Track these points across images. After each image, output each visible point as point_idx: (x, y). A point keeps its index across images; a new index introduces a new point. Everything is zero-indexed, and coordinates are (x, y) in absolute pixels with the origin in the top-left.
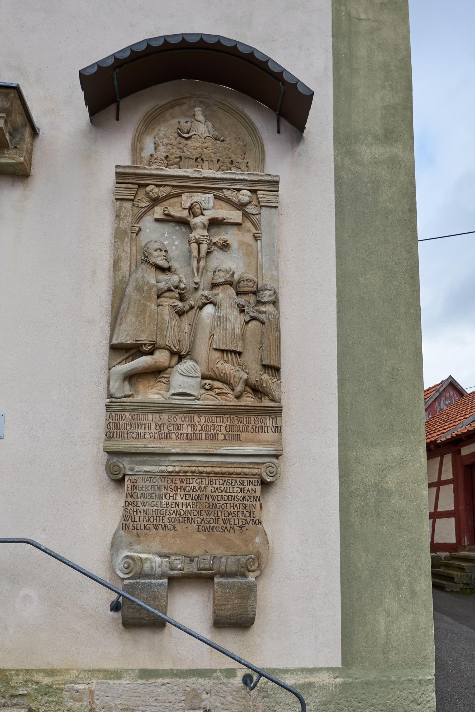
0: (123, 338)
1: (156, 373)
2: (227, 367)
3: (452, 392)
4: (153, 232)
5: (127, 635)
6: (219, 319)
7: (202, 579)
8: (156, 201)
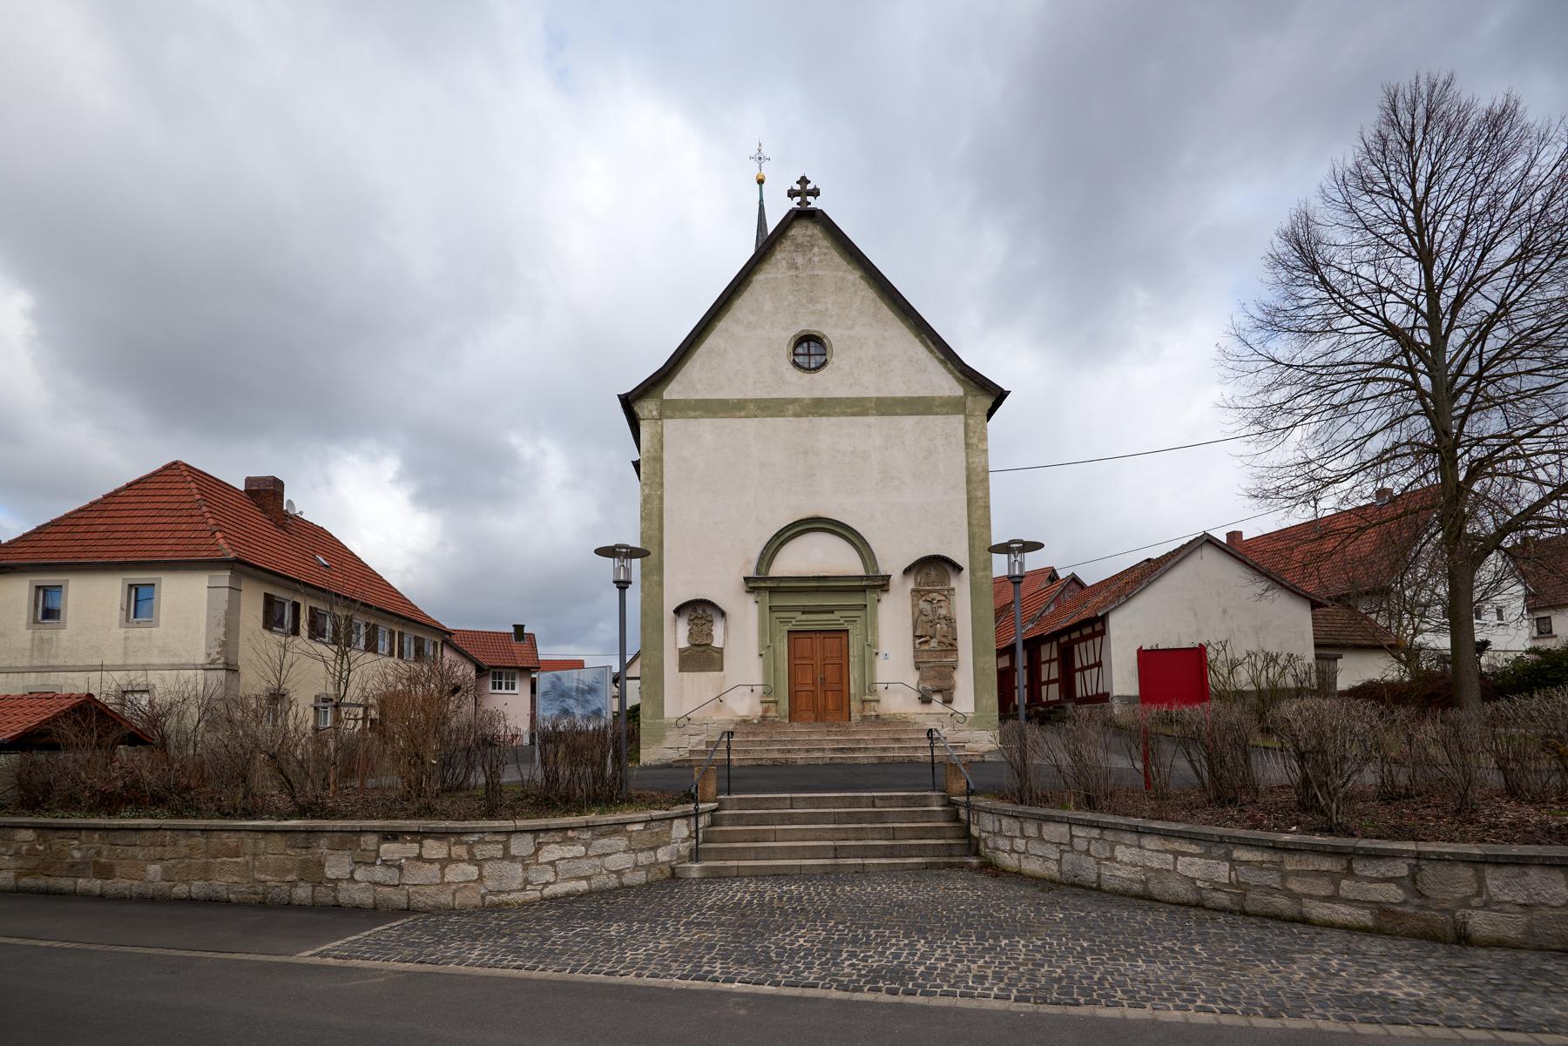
4: (922, 605)
6: (941, 627)
7: (939, 691)
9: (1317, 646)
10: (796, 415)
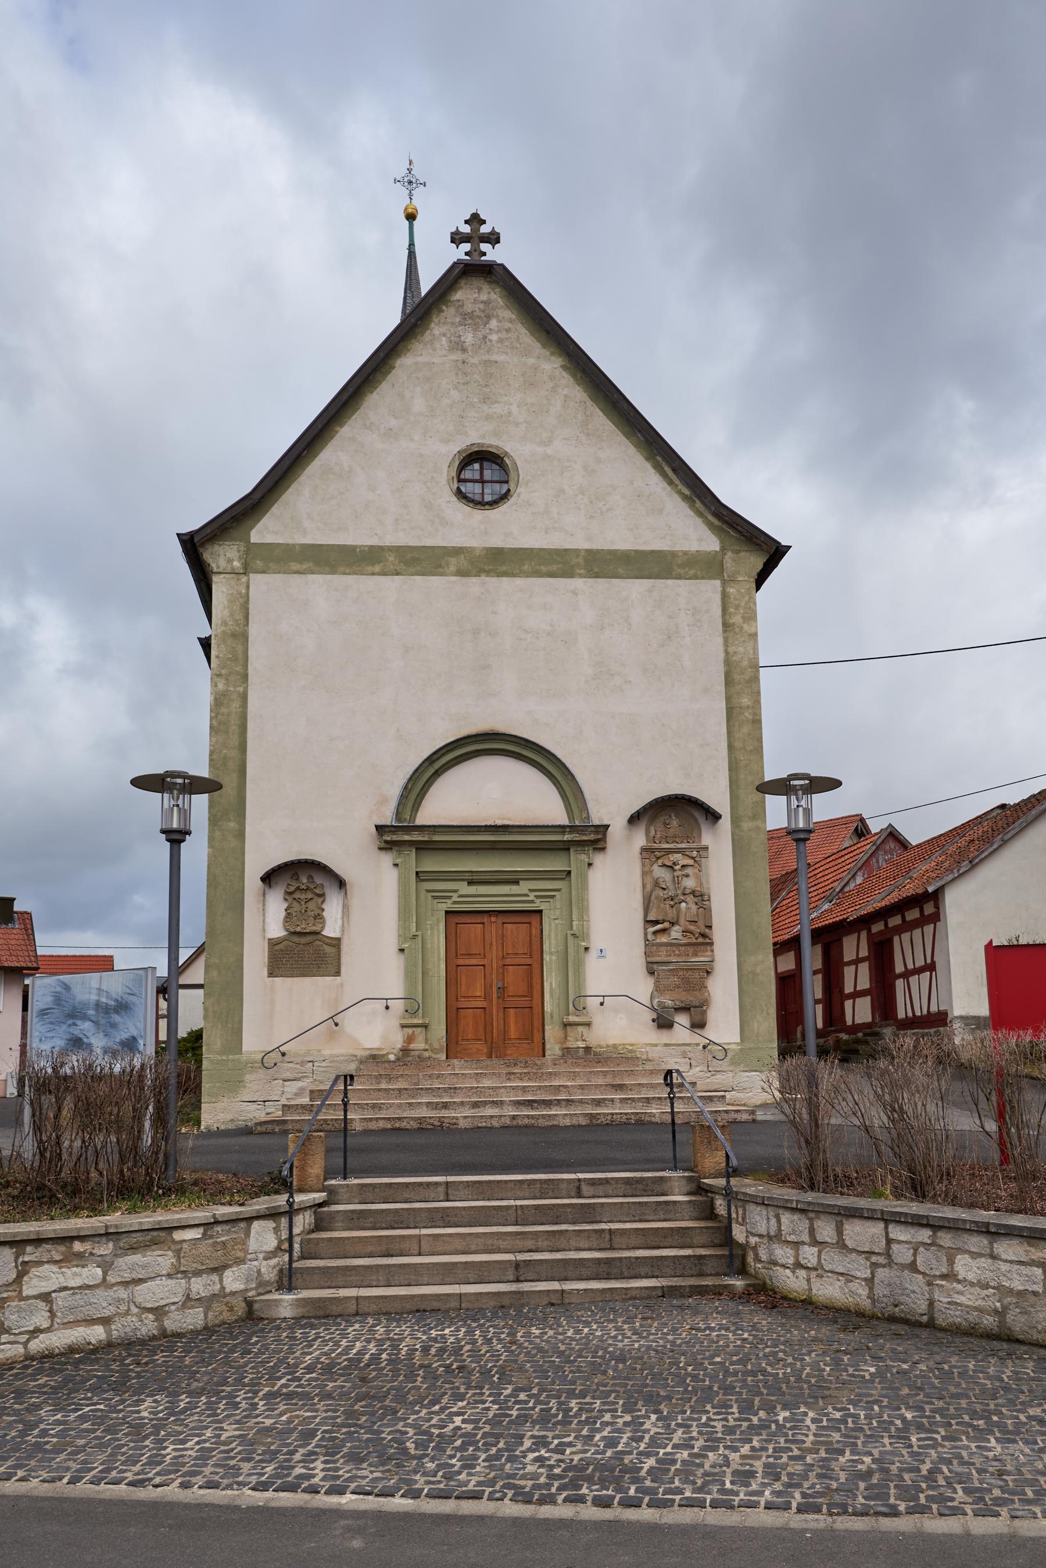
0: (651, 918)
1: (664, 931)
2: (692, 928)
3: (892, 844)
4: (659, 872)
5: (659, 1031)
8: (658, 858)
10: (462, 573)
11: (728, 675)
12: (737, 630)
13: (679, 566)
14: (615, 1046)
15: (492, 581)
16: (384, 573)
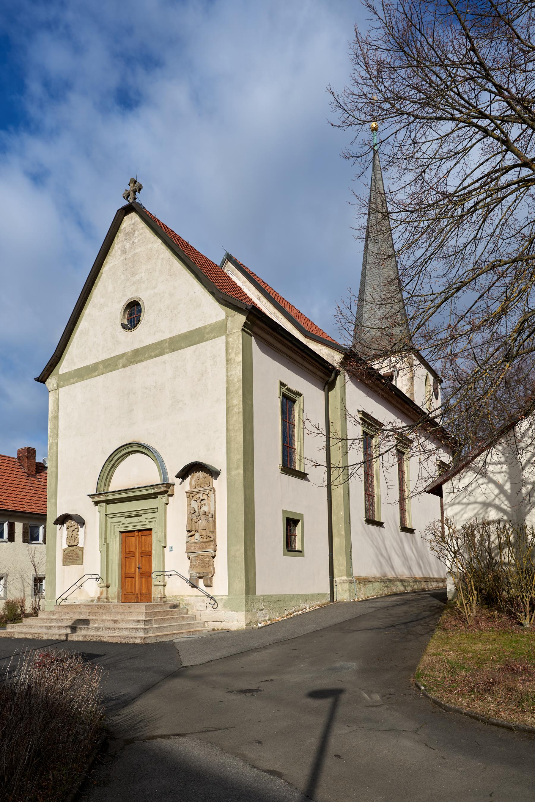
4: (194, 505)
9: (46, 515)
10: (124, 366)
11: (227, 389)
12: (232, 362)
13: (208, 334)
14: (175, 597)
15: (134, 367)
16: (98, 375)
